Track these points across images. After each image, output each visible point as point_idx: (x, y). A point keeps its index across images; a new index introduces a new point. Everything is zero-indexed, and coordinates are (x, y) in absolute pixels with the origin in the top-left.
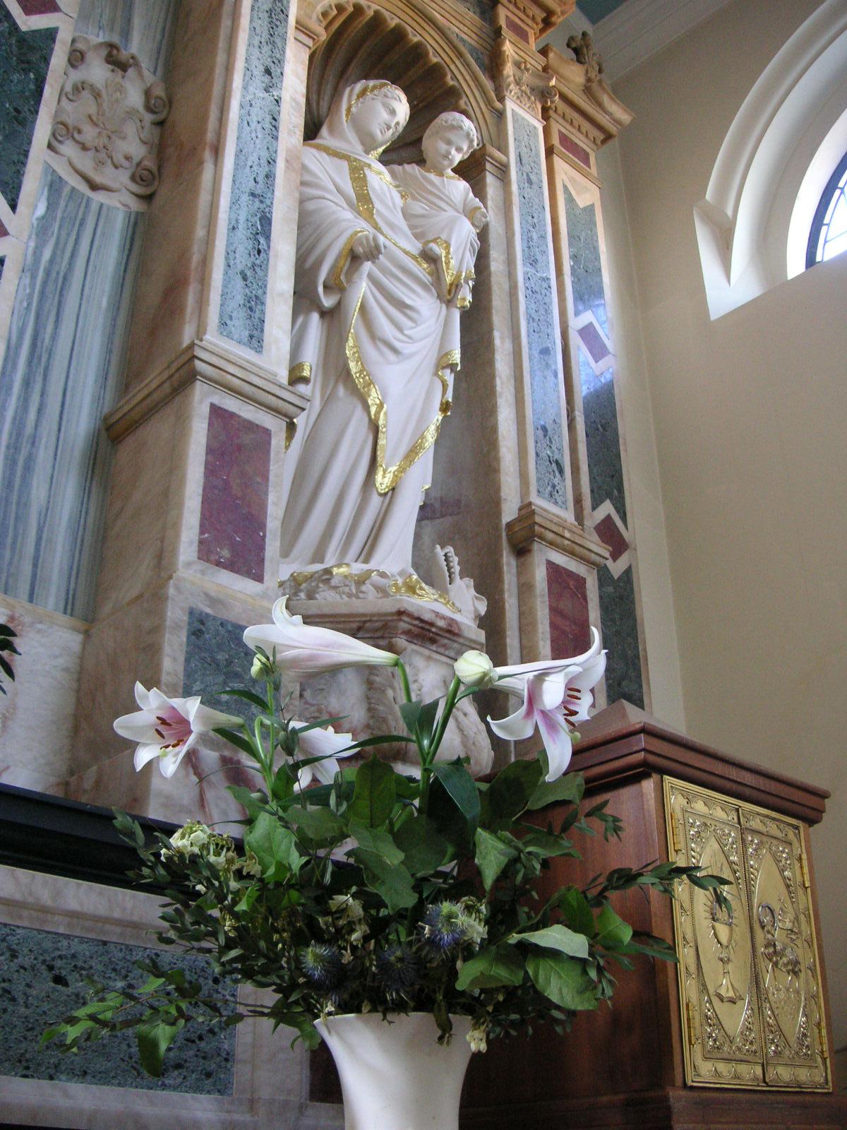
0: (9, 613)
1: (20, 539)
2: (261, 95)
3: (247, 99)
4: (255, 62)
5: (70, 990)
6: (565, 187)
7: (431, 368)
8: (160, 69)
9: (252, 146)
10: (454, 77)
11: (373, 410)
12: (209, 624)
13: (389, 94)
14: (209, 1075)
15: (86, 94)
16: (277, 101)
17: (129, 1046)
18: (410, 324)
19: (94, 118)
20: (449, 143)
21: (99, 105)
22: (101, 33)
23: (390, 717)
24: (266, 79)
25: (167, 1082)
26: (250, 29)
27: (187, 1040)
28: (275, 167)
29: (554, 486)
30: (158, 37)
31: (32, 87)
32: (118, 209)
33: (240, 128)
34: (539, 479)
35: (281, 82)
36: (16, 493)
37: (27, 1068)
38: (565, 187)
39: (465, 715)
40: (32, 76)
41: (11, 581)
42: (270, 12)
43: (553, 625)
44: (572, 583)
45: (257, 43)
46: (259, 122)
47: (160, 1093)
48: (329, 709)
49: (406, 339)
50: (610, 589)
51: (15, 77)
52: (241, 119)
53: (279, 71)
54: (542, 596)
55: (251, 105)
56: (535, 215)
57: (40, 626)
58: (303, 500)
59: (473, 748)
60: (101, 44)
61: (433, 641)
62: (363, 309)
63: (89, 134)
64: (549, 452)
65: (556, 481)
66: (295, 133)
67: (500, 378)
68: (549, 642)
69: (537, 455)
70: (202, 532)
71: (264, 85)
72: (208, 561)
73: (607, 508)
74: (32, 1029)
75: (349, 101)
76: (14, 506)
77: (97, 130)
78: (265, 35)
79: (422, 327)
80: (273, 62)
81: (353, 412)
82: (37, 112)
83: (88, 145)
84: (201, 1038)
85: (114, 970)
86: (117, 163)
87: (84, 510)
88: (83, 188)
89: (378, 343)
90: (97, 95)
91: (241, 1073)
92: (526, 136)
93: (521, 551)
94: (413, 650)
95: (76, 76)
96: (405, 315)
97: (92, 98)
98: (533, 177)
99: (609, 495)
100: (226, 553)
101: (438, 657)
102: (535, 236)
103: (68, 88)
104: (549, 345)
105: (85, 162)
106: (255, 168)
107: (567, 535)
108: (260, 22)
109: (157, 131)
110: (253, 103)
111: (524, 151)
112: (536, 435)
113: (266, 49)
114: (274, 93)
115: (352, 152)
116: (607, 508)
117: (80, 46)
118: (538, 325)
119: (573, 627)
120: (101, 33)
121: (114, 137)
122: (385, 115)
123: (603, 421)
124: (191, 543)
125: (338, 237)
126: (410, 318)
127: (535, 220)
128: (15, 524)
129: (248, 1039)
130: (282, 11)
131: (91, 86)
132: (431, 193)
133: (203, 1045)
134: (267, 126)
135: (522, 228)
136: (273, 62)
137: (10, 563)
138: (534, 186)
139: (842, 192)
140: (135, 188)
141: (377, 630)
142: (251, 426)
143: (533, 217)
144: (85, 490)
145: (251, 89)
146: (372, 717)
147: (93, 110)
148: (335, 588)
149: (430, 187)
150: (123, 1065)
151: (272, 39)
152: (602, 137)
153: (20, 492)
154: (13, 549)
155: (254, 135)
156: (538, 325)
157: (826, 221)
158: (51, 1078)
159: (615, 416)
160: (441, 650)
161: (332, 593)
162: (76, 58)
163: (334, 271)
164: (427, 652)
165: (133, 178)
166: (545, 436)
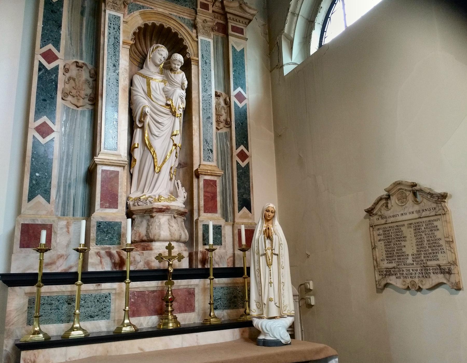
0: (67, 221)
1: (69, 203)
2: (113, 74)
3: (108, 77)
4: (110, 64)
5: (71, 305)
6: (233, 46)
7: (170, 136)
8: (93, 63)
9: (111, 92)
10: (181, 35)
11: (152, 153)
12: (102, 224)
13: (159, 50)
14: (104, 316)
15: (71, 81)
16: (118, 74)
17: (85, 313)
18: (162, 127)
19: (74, 88)
20: (175, 64)
21: (75, 83)
22: (74, 58)
23: (150, 233)
24: (114, 68)
25: (94, 319)
26: (108, 53)
27: (99, 310)
28: (118, 95)
29: (209, 157)
30: (92, 51)
31: (54, 86)
32: (86, 110)
33: (107, 88)
34: (204, 157)
35: (119, 67)
36: (67, 193)
37: (63, 322)
38: (233, 46)
39: (172, 227)
40: (54, 83)
41: (68, 213)
42: (113, 44)
43: (204, 196)
44: (211, 183)
45: (110, 57)
46: (112, 83)
47: (93, 321)
48: (139, 231)
49: (161, 131)
50: (241, 171)
51: (49, 85)
52: (107, 85)
53: (118, 63)
54: (202, 189)
55: (110, 79)
56: (207, 74)
57: (75, 222)
58: (141, 174)
59: (173, 235)
60: (74, 62)
61: (164, 212)
62: (149, 125)
63: (74, 92)
64: (208, 148)
65: (210, 155)
66: (126, 80)
67: (194, 130)
68: (203, 201)
69: (204, 149)
70: (101, 201)
71: (113, 71)
72: (103, 208)
73: (242, 147)
74: (63, 314)
75: (150, 54)
76: (67, 196)
77: (76, 90)
78: (113, 53)
79: (165, 127)
80: (116, 61)
81: (148, 154)
82: (57, 94)
83: (74, 96)
84: (102, 309)
85: (82, 299)
86: (83, 98)
87: (85, 192)
88: (75, 108)
89: (153, 135)
90: (74, 80)
91: (112, 314)
92: (205, 47)
93: (198, 177)
94: (159, 215)
95: (68, 75)
96: (161, 125)
97: (73, 81)
98: (207, 61)
99: (243, 144)
100: (108, 205)
101: (165, 214)
102: (207, 82)
103: (67, 80)
104: (210, 115)
105: (74, 101)
106: (112, 99)
107: (209, 171)
108: (110, 49)
109: (94, 82)
110: (110, 78)
111: (204, 53)
112: (204, 144)
113: (113, 58)
114: (117, 72)
115: (148, 75)
116: (242, 147)
117: (67, 67)
118: (206, 110)
119: (211, 194)
120: (74, 58)
121: (80, 91)
122: (160, 57)
123: (242, 122)
124: (98, 205)
125: (140, 108)
126: (162, 125)
127: (207, 76)
128: (68, 200)
129: (113, 308)
130: (118, 42)
131: (72, 78)
132: (171, 80)
133: (103, 310)
134: (115, 83)
135: (202, 81)
136: (116, 61)
137: (67, 209)
138: (208, 64)
139: (330, 19)
140: (90, 103)
141: (149, 212)
142: (113, 172)
143: (206, 75)
144: (85, 187)
145: (109, 74)
146: (147, 233)
147: (74, 85)
148: (142, 202)
149: (171, 79)
150: (84, 317)
151: (115, 54)
152: (247, 21)
153: (68, 192)
154: (68, 206)
155: (111, 88)
156: (206, 110)
157: (325, 30)
158: (68, 322)
159: (246, 119)
160: (167, 213)
161: (141, 203)
162: (66, 70)
163: (140, 118)
164: (162, 214)
165: (89, 100)
166: (207, 143)
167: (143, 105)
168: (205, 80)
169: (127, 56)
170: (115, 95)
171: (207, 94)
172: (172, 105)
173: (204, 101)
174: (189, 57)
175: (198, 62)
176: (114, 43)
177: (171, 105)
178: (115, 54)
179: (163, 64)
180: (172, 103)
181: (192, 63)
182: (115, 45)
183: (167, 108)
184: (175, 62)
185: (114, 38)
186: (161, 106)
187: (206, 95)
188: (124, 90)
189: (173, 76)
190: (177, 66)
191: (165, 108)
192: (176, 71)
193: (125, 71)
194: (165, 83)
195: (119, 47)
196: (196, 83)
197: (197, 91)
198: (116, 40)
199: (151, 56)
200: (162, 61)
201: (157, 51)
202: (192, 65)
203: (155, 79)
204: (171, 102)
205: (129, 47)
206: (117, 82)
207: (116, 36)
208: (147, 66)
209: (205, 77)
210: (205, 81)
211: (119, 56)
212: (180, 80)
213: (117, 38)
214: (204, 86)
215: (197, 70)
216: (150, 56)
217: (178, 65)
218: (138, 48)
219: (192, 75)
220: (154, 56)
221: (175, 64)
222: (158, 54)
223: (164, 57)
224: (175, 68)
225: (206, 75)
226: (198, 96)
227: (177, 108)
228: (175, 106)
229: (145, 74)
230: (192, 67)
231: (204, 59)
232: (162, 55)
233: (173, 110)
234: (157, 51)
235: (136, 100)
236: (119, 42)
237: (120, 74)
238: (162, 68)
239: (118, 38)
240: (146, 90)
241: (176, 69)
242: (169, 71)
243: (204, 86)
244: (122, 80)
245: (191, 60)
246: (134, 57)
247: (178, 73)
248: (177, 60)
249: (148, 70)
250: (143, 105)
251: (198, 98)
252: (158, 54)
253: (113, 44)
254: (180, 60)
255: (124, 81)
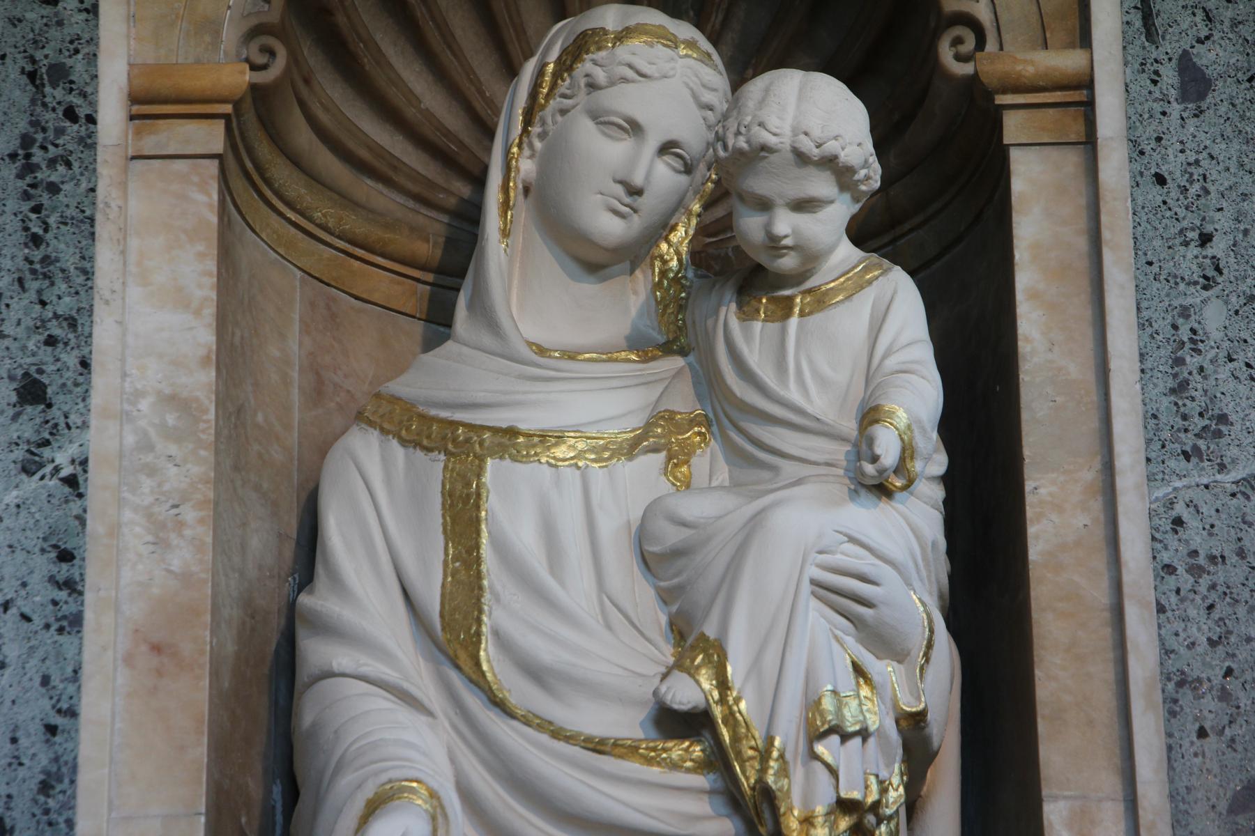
13: (600, 75)
16: (71, 481)
20: (765, 205)
28: (73, 735)
35: (85, 397)
53: (71, 359)
56: (1221, 223)
66: (180, 525)
80: (51, 341)
118: (1224, 695)
127: (1218, 247)
130: (71, 114)
135: (1144, 324)
136: (51, 341)
151: (37, 255)
156: (1224, 695)
167: (377, 774)
168: (1195, 297)
169: (200, 247)
170: (32, 741)
171: (1227, 478)
172: (730, 718)
173: (1186, 581)
174: (967, 69)
175: (1088, 107)
176: (27, 141)
177: (718, 711)
178: (37, 255)
179: (681, 234)
180: (723, 685)
181: (1014, 127)
182: (38, 156)
183: (675, 766)
184: (759, 184)
185: (32, 76)
186: (598, 746)
187: (1198, 496)
188: (157, 649)
189: (754, 357)
190: (785, 224)
191: (654, 773)
192: (797, 278)
193: (171, 419)
194: (677, 458)
195: (90, 169)
196: (1079, 369)
197: (1090, 474)
198: (55, 94)
199: (526, 167)
200: (651, 204)
201: (582, 97)
202: (1015, 154)
203: (548, 438)
204: (706, 681)
205: (212, 137)
206: (64, 571)
207: (47, 55)
208: (483, 310)
209: (1189, 261)
210: (1185, 312)
211: (88, 274)
212: (840, 376)
213: (59, 73)
214: (1181, 388)
215: (1074, 206)
216: (507, 169)
217: (803, 205)
218: (410, 112)
219: (1024, 279)
220: (551, 162)
221: (765, 205)
222: (586, 134)
223: (667, 148)
224: (774, 244)
225: (1205, 239)
226: (1099, 533)
227: (787, 736)
228: (759, 734)
229: (443, 395)
230: (1018, 185)
231: (1171, 46)
232: (634, 128)
233: (747, 779)
234: (582, 97)
235: (316, 727)
236: (82, 112)
237: (98, 481)
238: (676, 280)
239: (78, 65)
240: (431, 596)
241: (788, 262)
242: (729, 294)
243: (1181, 388)
244: (136, 535)
245: (989, 95)
246: (354, 224)
247: (820, 300)
248: (764, 148)
249: (487, 340)
250: (377, 774)
251: (1100, 562)
252: (586, 134)
253: (14, 144)
254: (807, 145)
255: (160, 543)
